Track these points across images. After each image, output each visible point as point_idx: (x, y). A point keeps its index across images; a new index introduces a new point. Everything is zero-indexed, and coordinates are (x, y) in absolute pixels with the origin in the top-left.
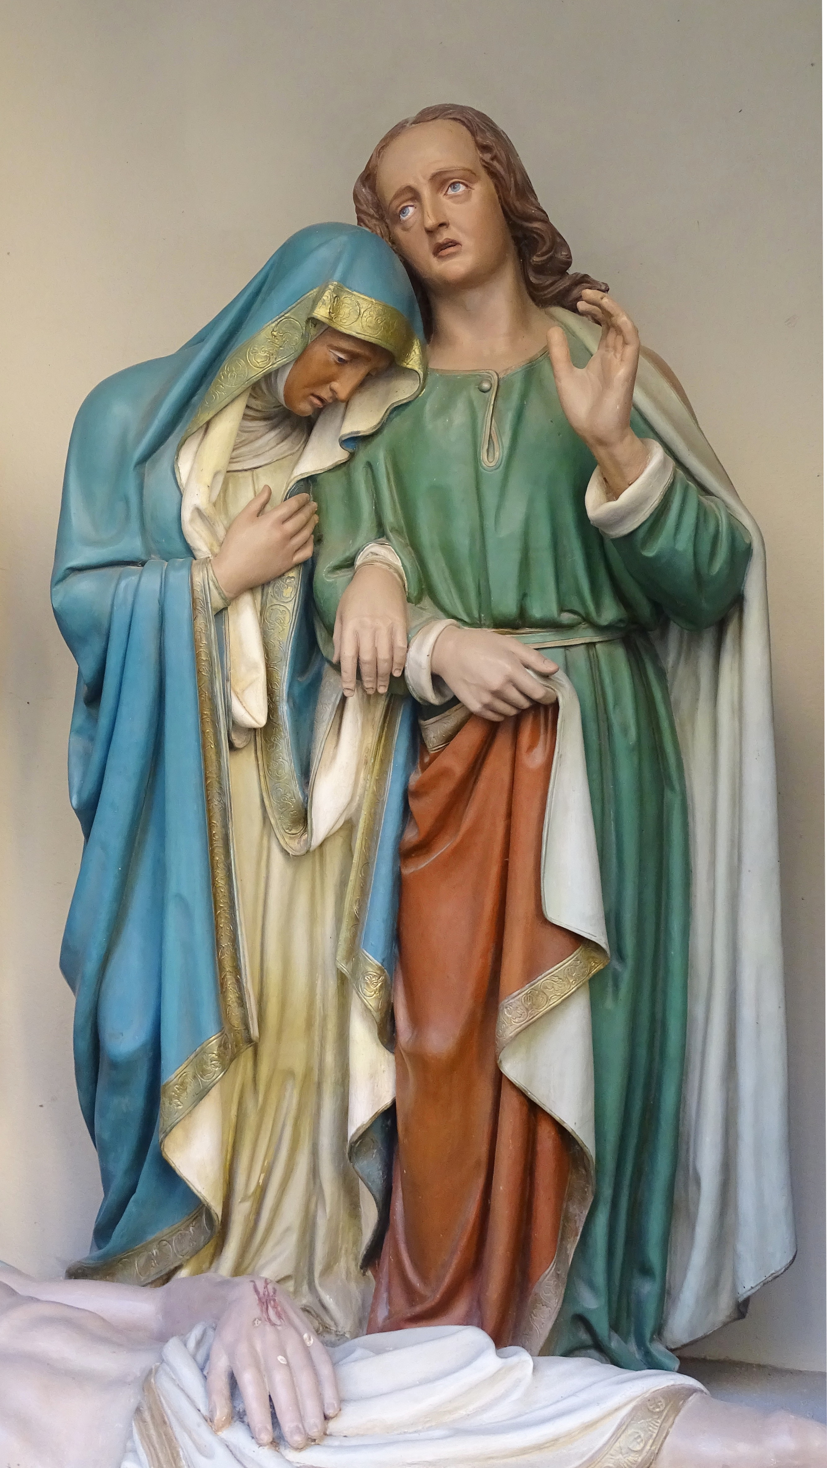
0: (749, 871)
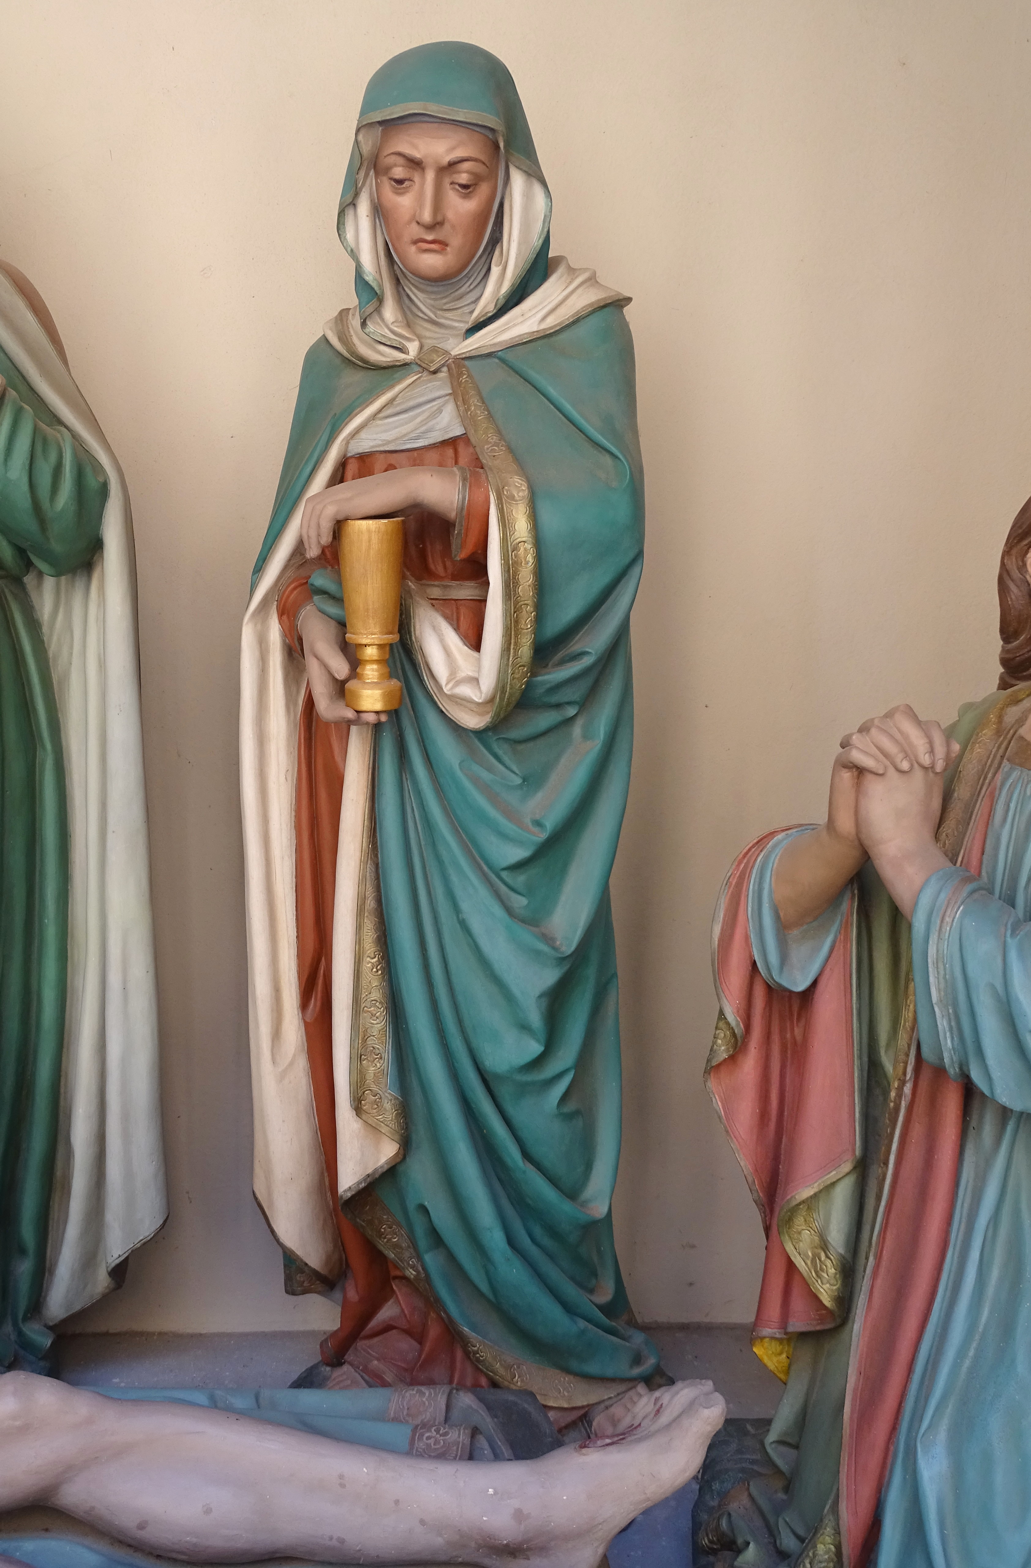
0: (113, 832)
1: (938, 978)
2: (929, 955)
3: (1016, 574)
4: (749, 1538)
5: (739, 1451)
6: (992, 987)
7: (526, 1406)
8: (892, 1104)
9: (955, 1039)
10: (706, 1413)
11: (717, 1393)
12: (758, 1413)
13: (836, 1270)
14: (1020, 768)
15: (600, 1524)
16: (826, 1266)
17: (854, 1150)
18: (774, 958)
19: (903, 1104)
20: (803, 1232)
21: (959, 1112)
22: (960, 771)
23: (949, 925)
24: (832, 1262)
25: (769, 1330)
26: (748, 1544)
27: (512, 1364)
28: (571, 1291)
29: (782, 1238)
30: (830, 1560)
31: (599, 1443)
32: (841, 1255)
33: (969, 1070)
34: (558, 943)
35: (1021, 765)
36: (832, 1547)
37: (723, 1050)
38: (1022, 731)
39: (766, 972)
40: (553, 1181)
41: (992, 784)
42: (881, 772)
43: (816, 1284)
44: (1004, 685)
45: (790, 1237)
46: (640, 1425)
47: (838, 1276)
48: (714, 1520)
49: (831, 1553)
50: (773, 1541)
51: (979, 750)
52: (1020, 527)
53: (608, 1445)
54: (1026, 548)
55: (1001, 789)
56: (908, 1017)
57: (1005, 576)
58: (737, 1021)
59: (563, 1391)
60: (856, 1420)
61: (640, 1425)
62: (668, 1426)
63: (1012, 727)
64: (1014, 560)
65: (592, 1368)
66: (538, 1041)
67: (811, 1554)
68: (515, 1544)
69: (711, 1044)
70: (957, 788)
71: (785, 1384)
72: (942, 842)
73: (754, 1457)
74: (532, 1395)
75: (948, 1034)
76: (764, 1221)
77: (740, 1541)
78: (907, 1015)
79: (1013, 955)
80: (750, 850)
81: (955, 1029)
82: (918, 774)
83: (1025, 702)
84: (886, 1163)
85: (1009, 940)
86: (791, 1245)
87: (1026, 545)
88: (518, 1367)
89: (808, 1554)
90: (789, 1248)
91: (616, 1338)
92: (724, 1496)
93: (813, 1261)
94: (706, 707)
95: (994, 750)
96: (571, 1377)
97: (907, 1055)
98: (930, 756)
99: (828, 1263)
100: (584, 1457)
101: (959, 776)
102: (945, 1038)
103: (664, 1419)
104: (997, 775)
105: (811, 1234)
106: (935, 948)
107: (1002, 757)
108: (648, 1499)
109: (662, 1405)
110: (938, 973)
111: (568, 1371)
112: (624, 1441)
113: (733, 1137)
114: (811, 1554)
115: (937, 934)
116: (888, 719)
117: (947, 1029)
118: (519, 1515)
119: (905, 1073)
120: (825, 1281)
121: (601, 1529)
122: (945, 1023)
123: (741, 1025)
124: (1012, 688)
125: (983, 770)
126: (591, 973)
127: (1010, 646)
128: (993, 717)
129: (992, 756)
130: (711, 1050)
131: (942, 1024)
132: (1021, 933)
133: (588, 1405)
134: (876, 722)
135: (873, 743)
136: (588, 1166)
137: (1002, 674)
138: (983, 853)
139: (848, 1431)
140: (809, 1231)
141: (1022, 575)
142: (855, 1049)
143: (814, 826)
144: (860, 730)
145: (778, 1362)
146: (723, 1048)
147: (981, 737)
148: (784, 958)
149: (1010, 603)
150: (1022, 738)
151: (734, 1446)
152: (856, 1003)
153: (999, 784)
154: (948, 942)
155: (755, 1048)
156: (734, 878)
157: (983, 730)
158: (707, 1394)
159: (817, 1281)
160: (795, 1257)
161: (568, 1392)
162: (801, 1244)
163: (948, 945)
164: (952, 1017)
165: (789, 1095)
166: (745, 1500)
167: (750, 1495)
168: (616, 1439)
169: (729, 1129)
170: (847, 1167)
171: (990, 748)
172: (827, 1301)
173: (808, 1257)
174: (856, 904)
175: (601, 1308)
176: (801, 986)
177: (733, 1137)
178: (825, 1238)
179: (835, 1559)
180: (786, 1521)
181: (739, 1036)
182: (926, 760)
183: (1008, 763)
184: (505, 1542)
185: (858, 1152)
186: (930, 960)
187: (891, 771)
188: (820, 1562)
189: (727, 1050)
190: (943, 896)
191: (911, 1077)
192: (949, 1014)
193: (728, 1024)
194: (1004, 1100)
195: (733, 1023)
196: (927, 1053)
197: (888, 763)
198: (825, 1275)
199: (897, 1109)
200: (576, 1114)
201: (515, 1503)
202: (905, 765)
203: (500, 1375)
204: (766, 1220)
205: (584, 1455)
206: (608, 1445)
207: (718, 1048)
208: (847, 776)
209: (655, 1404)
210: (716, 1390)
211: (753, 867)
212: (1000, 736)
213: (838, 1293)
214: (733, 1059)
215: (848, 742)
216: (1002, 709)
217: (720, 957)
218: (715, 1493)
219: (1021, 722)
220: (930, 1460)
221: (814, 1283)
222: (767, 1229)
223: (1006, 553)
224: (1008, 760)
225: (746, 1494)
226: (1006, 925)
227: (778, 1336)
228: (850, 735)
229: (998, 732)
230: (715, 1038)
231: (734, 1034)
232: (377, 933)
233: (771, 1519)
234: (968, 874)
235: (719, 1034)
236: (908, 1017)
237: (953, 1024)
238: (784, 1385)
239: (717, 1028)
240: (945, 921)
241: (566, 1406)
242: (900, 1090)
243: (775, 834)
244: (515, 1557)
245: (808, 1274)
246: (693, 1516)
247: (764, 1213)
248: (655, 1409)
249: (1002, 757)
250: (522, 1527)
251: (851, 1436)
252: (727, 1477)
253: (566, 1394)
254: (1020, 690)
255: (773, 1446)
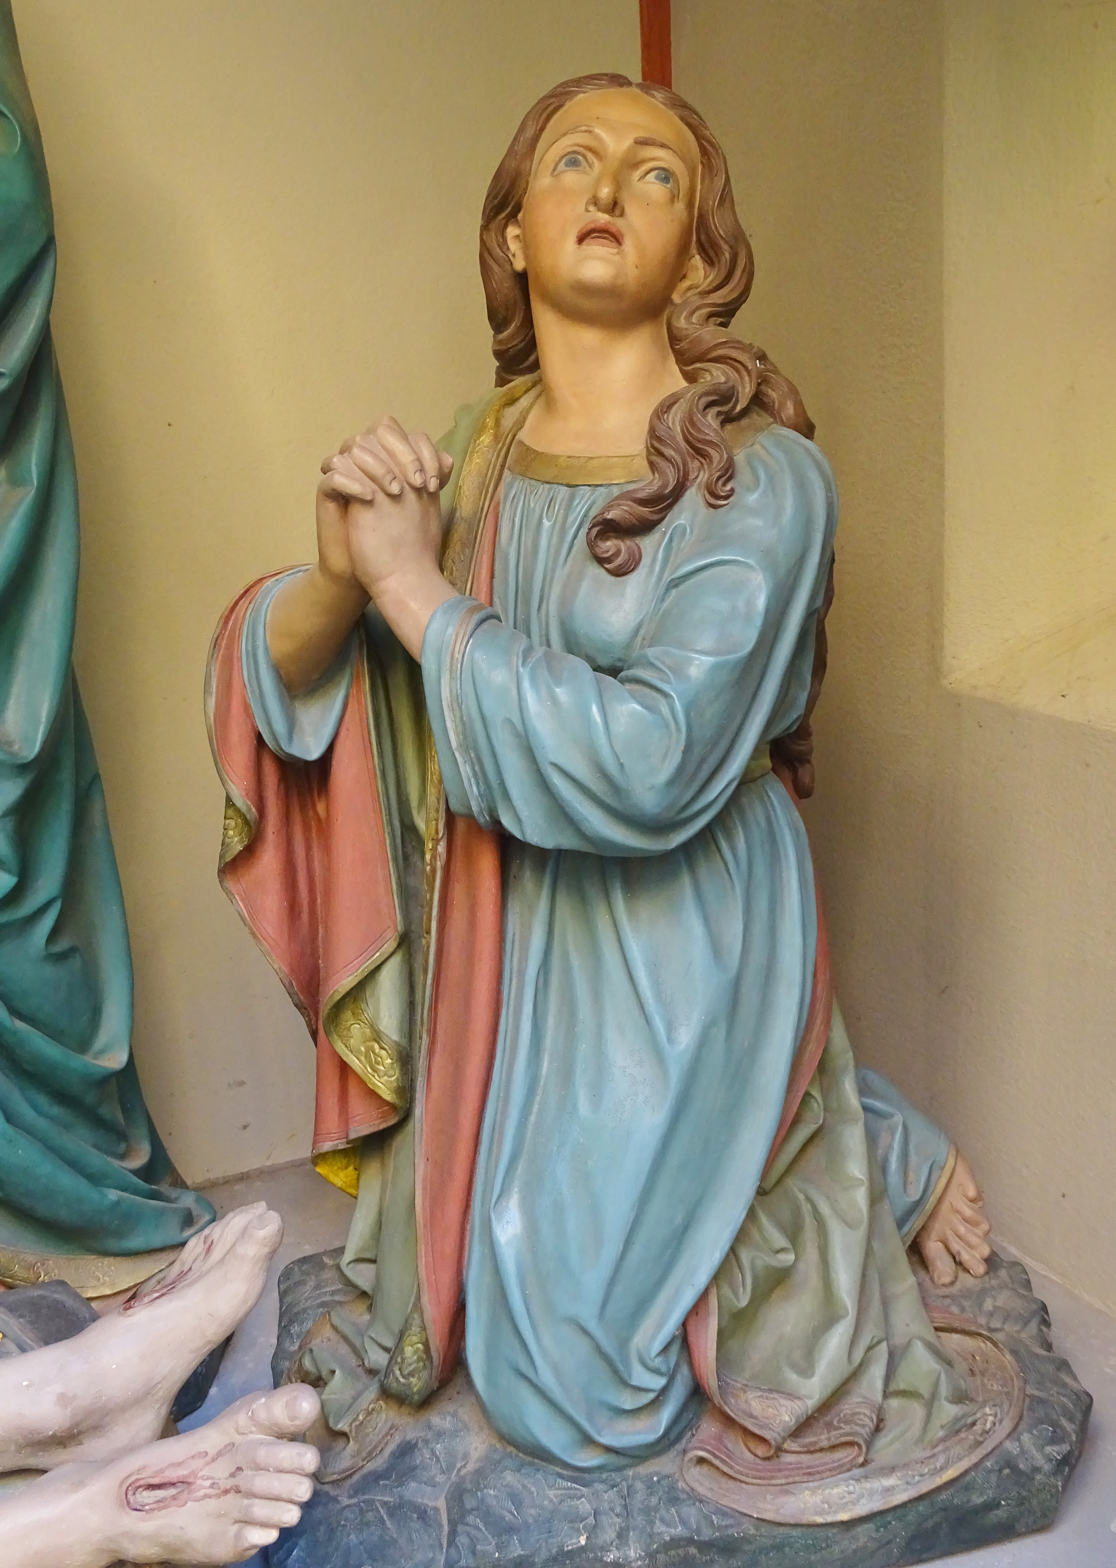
1: (455, 722)
2: (443, 698)
3: (497, 251)
4: (334, 1366)
5: (318, 1287)
6: (510, 721)
7: (56, 1296)
8: (428, 868)
9: (481, 785)
10: (262, 1233)
11: (271, 1211)
12: (337, 1244)
13: (391, 1059)
14: (521, 477)
15: (159, 1383)
16: (381, 1058)
17: (396, 927)
18: (280, 727)
19: (439, 864)
20: (353, 1026)
21: (496, 863)
22: (461, 487)
23: (460, 661)
24: (387, 1053)
25: (331, 1143)
26: (333, 1372)
27: (34, 1262)
28: (96, 1159)
29: (330, 1038)
30: (420, 1359)
31: (146, 1300)
32: (396, 1041)
33: (498, 816)
34: (16, 747)
35: (521, 475)
36: (420, 1346)
37: (237, 842)
38: (522, 435)
39: (274, 743)
40: (55, 1034)
41: (495, 498)
42: (369, 498)
43: (373, 1079)
44: (501, 382)
45: (339, 1036)
46: (190, 1268)
47: (395, 1065)
48: (295, 1363)
49: (419, 1352)
50: (361, 1363)
51: (478, 461)
52: (495, 197)
53: (156, 1299)
54: (504, 221)
55: (505, 503)
56: (435, 769)
57: (486, 255)
58: (247, 805)
59: (103, 1277)
60: (428, 1209)
61: (190, 1268)
62: (222, 1260)
63: (510, 431)
64: (493, 235)
65: (135, 1242)
66: (9, 872)
67: (399, 1360)
68: (62, 1432)
69: (222, 838)
70: (459, 506)
71: (356, 1198)
72: (449, 570)
73: (333, 1288)
74: (62, 1283)
75: (473, 781)
76: (309, 1024)
77: (325, 1373)
78: (432, 767)
79: (526, 684)
80: (236, 603)
81: (479, 774)
82: (411, 497)
83: (522, 400)
84: (428, 932)
85: (521, 669)
86: (341, 1044)
87: (504, 218)
88: (43, 1265)
89: (396, 1361)
90: (340, 1048)
91: (159, 1202)
92: (306, 1338)
93: (367, 1056)
94: (169, 425)
95: (493, 460)
96: (111, 1259)
97: (437, 811)
98: (421, 474)
99: (383, 1052)
100: (131, 1318)
101: (460, 493)
102: (471, 785)
103: (217, 1254)
104: (499, 488)
105: (361, 1028)
106: (448, 690)
107: (503, 466)
108: (209, 1342)
109: (212, 1241)
110: (455, 716)
111: (106, 1253)
112: (174, 1290)
113: (261, 938)
114: (399, 1360)
115: (448, 672)
116: (371, 436)
117: (471, 775)
118: (63, 1399)
119: (437, 832)
120: (381, 1074)
121: (160, 1389)
122: (468, 769)
123: (254, 810)
124: (507, 386)
125: (484, 484)
126: (66, 777)
127: (501, 336)
128: (490, 422)
129: (492, 466)
130: (223, 844)
131: (465, 770)
132: (533, 660)
133: (135, 1286)
134: (358, 439)
135: (355, 464)
136: (96, 1012)
137: (498, 368)
138: (492, 577)
139: (422, 1221)
140: (359, 1024)
141: (503, 252)
142: (384, 814)
143: (308, 567)
144: (342, 452)
145: (346, 1177)
146: (236, 839)
147: (479, 445)
148: (292, 723)
149: (495, 286)
150: (521, 443)
151: (311, 1283)
152: (379, 764)
153: (502, 497)
154: (461, 681)
155: (274, 833)
156: (223, 639)
157: (479, 438)
158: (261, 1216)
159: (374, 1076)
160: (347, 1055)
161: (110, 1276)
162: (352, 1041)
163: (461, 684)
164: (475, 761)
165: (318, 880)
166: (328, 1332)
167: (334, 1328)
168: (165, 1290)
169: (256, 931)
170: (390, 945)
171: (489, 457)
172: (388, 1095)
173: (359, 1051)
174: (365, 650)
175: (136, 1172)
176: (314, 753)
177: (261, 938)
178: (377, 1028)
179: (425, 1357)
180: (371, 1338)
181: (252, 824)
182: (417, 480)
183: (509, 472)
184: (51, 1433)
185: (400, 927)
186: (444, 703)
187: (381, 497)
188: (410, 1365)
189: (241, 841)
190: (450, 630)
191: (443, 834)
192: (471, 758)
193: (238, 811)
194: (535, 840)
195: (244, 809)
196: (455, 806)
197: (375, 487)
198: (381, 1068)
199: (434, 871)
200: (72, 951)
201: (57, 1388)
202: (395, 488)
203: (20, 1278)
204: (311, 1024)
205: (130, 1316)
206: (156, 1299)
207: (230, 840)
208: (331, 507)
209: (205, 1243)
210: (269, 1209)
211: (242, 623)
212: (499, 443)
213: (398, 1084)
214: (250, 851)
215: (329, 466)
216: (498, 411)
217: (218, 734)
218: (295, 1337)
219: (520, 424)
220: (505, 1226)
221: (370, 1079)
222: (314, 1034)
223: (485, 228)
224: (509, 469)
225: (328, 1326)
226: (518, 655)
227: (341, 1147)
228: (330, 458)
229: (496, 438)
230: (225, 829)
231: (246, 821)
232: (639, 522)
233: (358, 1343)
234: (474, 603)
235: (229, 824)
236: (435, 769)
237: (477, 768)
238: (354, 1200)
239: (225, 818)
240: (455, 659)
241: (108, 1292)
242: (434, 849)
243: (264, 581)
244: (65, 1447)
245: (363, 1071)
246: (273, 1368)
247: (309, 1015)
248: (206, 1248)
249: (503, 466)
250: (68, 1411)
251: (425, 1226)
252: (305, 1315)
253: (107, 1279)
254: (515, 387)
255: (351, 1266)
